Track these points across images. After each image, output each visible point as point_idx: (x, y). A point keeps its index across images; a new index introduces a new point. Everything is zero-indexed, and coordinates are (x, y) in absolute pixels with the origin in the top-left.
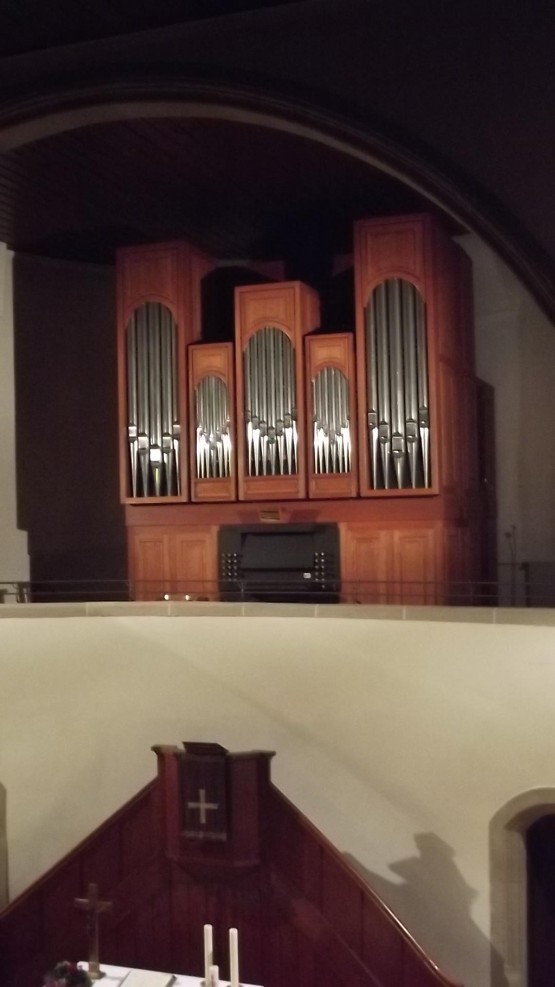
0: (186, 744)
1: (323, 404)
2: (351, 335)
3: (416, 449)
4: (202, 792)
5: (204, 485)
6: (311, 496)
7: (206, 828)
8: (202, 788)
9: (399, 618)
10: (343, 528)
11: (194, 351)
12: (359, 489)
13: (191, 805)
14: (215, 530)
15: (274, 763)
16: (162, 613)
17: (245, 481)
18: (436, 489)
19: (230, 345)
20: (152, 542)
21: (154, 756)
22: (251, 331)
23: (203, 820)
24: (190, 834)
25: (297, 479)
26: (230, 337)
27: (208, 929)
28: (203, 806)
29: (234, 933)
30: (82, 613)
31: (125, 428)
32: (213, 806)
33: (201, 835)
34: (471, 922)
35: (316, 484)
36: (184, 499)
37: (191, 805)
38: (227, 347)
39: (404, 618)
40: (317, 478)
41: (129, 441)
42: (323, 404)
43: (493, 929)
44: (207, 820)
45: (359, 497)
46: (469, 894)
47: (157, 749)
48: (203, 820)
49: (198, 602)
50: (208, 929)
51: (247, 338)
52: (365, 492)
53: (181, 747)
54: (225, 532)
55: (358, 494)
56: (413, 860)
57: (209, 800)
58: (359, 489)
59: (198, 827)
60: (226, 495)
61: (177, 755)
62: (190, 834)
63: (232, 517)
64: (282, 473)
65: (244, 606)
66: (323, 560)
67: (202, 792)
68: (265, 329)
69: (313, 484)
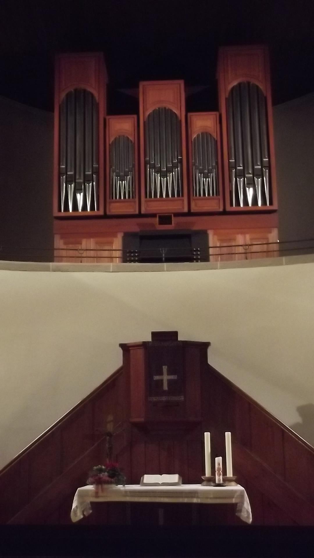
1: (199, 157)
2: (135, 116)
3: (261, 182)
4: (165, 368)
5: (118, 204)
7: (169, 393)
8: (165, 365)
9: (281, 264)
10: (211, 233)
11: (110, 120)
13: (156, 378)
21: (120, 351)
22: (149, 111)
23: (165, 387)
24: (154, 399)
25: (183, 200)
26: (137, 112)
27: (207, 435)
28: (166, 378)
29: (228, 435)
30: (47, 269)
32: (172, 377)
33: (164, 399)
36: (101, 213)
37: (156, 378)
40: (194, 199)
44: (168, 387)
45: (225, 213)
47: (124, 347)
48: (165, 387)
50: (207, 435)
52: (228, 209)
53: (149, 339)
54: (128, 237)
59: (164, 393)
61: (144, 344)
62: (154, 399)
63: (133, 226)
64: (176, 196)
65: (165, 265)
66: (199, 253)
67: (165, 368)
68: (146, 197)
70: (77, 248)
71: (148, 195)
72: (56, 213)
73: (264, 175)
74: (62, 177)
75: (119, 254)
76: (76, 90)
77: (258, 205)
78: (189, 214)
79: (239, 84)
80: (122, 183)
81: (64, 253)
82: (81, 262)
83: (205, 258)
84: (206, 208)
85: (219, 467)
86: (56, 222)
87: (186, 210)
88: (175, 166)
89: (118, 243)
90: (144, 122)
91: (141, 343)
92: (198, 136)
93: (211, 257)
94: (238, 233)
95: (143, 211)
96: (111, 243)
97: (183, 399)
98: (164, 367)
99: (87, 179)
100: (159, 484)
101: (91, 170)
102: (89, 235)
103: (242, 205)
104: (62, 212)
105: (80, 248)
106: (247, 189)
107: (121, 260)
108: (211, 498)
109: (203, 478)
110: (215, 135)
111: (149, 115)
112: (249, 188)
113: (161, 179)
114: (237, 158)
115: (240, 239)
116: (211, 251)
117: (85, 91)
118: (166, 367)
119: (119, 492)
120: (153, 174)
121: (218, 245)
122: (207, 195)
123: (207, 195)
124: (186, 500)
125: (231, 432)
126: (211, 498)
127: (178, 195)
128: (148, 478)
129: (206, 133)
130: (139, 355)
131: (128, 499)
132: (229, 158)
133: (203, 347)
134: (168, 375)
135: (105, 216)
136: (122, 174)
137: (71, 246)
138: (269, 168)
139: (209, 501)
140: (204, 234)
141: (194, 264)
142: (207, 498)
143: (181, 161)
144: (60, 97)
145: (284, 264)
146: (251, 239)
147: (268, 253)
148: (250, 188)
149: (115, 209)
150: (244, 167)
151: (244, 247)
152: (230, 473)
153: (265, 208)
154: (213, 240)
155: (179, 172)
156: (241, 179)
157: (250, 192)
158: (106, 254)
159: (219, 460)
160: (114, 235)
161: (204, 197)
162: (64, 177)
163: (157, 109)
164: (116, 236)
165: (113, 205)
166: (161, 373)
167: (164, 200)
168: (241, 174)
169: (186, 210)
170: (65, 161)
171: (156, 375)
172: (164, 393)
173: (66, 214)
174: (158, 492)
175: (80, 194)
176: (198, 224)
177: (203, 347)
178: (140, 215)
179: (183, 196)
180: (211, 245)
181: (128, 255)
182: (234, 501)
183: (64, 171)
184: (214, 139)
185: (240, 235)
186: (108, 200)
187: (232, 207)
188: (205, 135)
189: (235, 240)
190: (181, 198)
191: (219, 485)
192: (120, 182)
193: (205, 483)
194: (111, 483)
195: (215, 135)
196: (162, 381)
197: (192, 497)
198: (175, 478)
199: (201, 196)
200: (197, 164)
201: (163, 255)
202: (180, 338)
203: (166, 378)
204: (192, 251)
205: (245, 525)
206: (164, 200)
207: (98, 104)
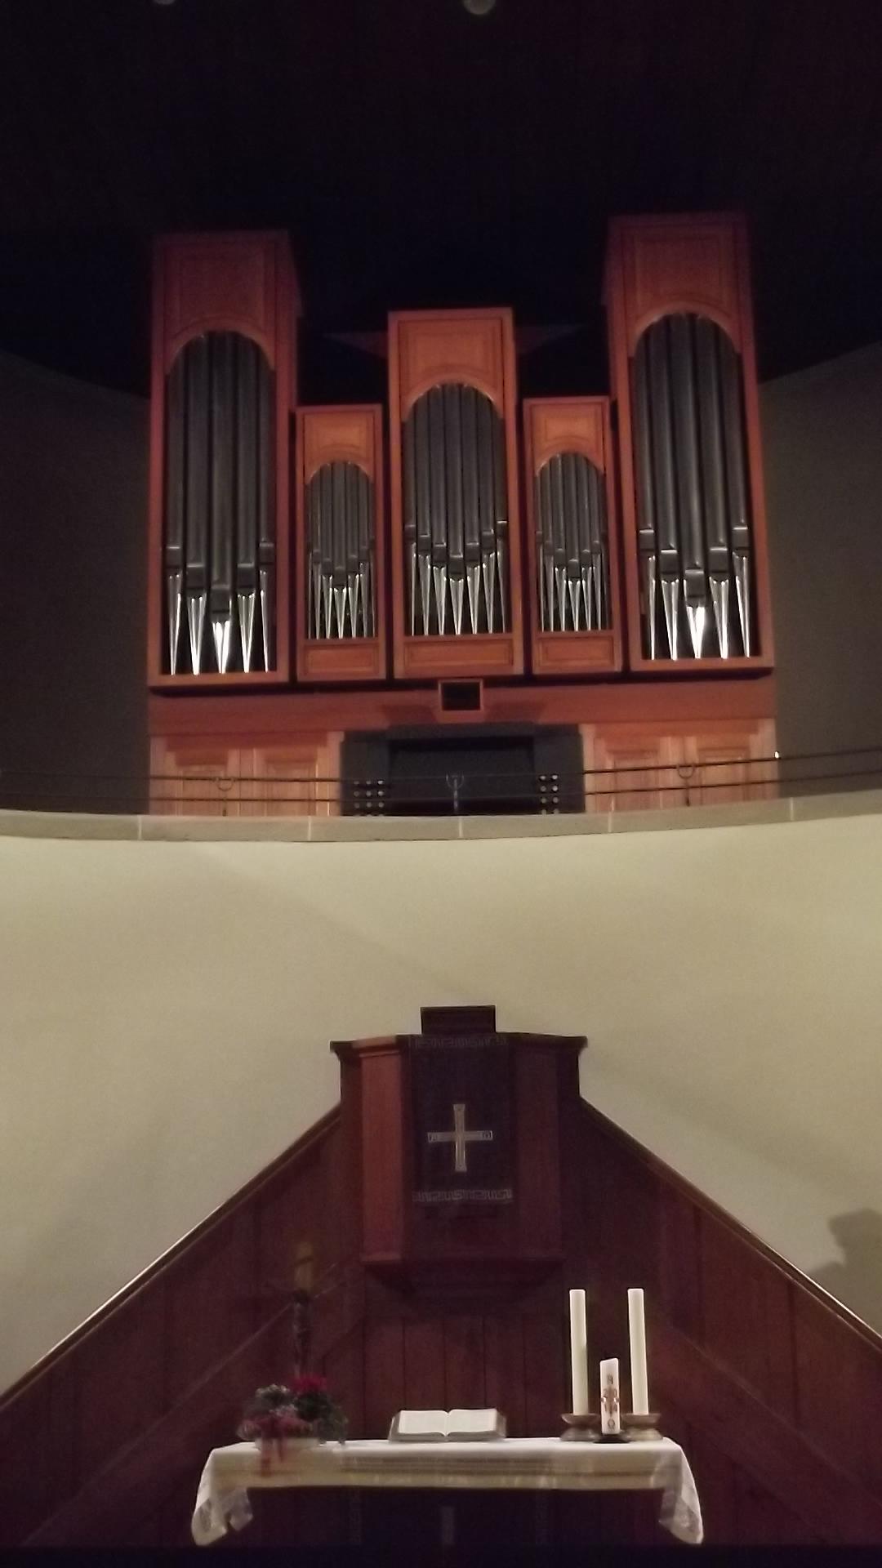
0: (430, 1016)
1: (555, 522)
4: (459, 1111)
6: (537, 671)
7: (471, 1179)
8: (460, 1101)
10: (588, 732)
13: (435, 1137)
14: (335, 740)
16: (296, 836)
17: (407, 645)
19: (378, 408)
20: (605, 469)
21: (335, 1063)
23: (461, 1163)
24: (427, 1197)
27: (577, 1298)
28: (461, 1137)
29: (636, 1297)
30: (130, 835)
32: (479, 1136)
33: (457, 1196)
35: (546, 651)
36: (282, 675)
37: (435, 1137)
38: (372, 411)
39: (792, 816)
42: (555, 522)
45: (627, 676)
47: (342, 1049)
48: (461, 1163)
49: (638, 616)
50: (577, 1298)
52: (638, 664)
53: (414, 1027)
54: (355, 743)
57: (470, 1125)
59: (458, 1181)
60: (365, 669)
61: (402, 1044)
63: (371, 713)
65: (460, 822)
67: (459, 1111)
72: (155, 678)
73: (737, 570)
74: (171, 577)
75: (331, 790)
76: (211, 335)
78: (529, 679)
79: (667, 321)
80: (341, 593)
81: (178, 789)
83: (573, 803)
87: (518, 669)
88: (487, 546)
89: (328, 760)
90: (403, 426)
91: (394, 1041)
92: (552, 462)
94: (664, 734)
95: (399, 672)
96: (310, 761)
97: (508, 1194)
98: (456, 1107)
99: (244, 583)
100: (443, 1435)
102: (248, 739)
106: (689, 609)
108: (586, 1475)
110: (601, 460)
112: (695, 607)
115: (671, 750)
116: (590, 783)
119: (329, 1458)
124: (517, 1482)
126: (586, 1475)
127: (603, 626)
128: (410, 1421)
129: (576, 455)
130: (386, 1076)
133: (567, 1051)
135: (294, 687)
139: (584, 1484)
140: (568, 736)
141: (544, 817)
142: (578, 1475)
143: (504, 533)
146: (701, 750)
147: (747, 788)
148: (697, 607)
149: (320, 665)
152: (641, 1405)
153: (738, 664)
154: (593, 751)
157: (222, 634)
158: (295, 790)
159: (609, 1367)
160: (319, 737)
161: (570, 634)
162: (178, 576)
163: (438, 386)
165: (316, 656)
166: (447, 1124)
167: (459, 642)
168: (673, 569)
169: (518, 669)
170: (180, 531)
171: (436, 1130)
172: (458, 1181)
173: (183, 680)
174: (440, 1460)
175: (223, 622)
176: (553, 706)
177: (567, 1051)
178: (390, 684)
179: (509, 628)
180: (588, 764)
182: (652, 1482)
183: (178, 561)
184: (597, 471)
185: (669, 738)
186: (301, 641)
188: (572, 461)
189: (655, 751)
192: (336, 590)
195: (601, 460)
196: (451, 1145)
197: (535, 1473)
198: (486, 1419)
200: (550, 542)
202: (503, 1026)
203: (461, 1137)
206: (459, 642)
207: (273, 375)
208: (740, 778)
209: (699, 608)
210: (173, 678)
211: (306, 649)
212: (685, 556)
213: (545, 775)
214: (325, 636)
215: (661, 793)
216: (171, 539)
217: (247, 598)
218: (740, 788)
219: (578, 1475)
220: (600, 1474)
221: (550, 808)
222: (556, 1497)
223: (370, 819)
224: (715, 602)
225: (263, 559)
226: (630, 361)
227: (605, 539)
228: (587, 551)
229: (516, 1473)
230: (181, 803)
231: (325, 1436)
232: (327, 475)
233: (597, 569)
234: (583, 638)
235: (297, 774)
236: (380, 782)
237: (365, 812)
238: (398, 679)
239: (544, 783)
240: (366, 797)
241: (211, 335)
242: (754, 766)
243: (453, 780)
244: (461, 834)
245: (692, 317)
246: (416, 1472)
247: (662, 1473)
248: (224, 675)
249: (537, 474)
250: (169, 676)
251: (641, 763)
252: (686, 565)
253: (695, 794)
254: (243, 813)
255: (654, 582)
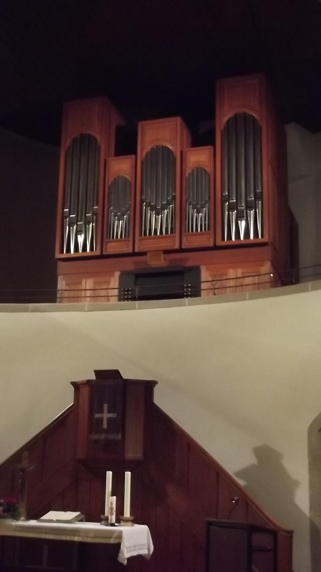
0: (98, 373)
2: (211, 147)
4: (106, 406)
7: (107, 431)
9: (244, 299)
12: (215, 240)
13: (97, 416)
14: (117, 274)
15: (157, 390)
16: (81, 310)
17: (140, 240)
18: (266, 239)
19: (133, 156)
21: (72, 389)
22: (148, 149)
23: (105, 426)
24: (94, 437)
25: (174, 237)
27: (109, 474)
28: (106, 415)
29: (128, 475)
30: (27, 310)
31: (61, 211)
32: (111, 415)
33: (103, 437)
34: (296, 506)
37: (97, 416)
38: (131, 158)
41: (63, 217)
43: (311, 508)
45: (216, 248)
46: (296, 484)
47: (74, 384)
48: (105, 426)
50: (109, 474)
51: (145, 153)
52: (219, 243)
53: (93, 377)
54: (124, 275)
55: (215, 244)
56: (253, 466)
58: (215, 240)
61: (89, 382)
62: (94, 437)
63: (129, 264)
65: (137, 303)
67: (106, 406)
69: (184, 240)
70: (78, 289)
71: (143, 233)
72: (58, 255)
73: (257, 206)
74: (65, 220)
75: (116, 292)
76: (81, 135)
77: (250, 238)
78: (181, 250)
79: (236, 116)
80: (199, 215)
81: (66, 294)
82: (61, 302)
83: (196, 293)
84: (196, 244)
85: (111, 507)
86: (60, 264)
88: (168, 204)
89: (115, 282)
90: (142, 162)
91: (86, 382)
92: (193, 170)
93: (202, 292)
94: (230, 268)
95: (136, 250)
96: (108, 282)
97: (120, 437)
98: (105, 405)
99: (250, 206)
100: (53, 520)
101: (91, 212)
102: (89, 274)
103: (233, 239)
104: (64, 253)
105: (80, 288)
106: (239, 222)
107: (116, 298)
108: (91, 537)
109: (102, 517)
110: (209, 169)
111: (147, 154)
112: (241, 221)
113: (155, 217)
114: (230, 192)
115: (231, 273)
116: (203, 286)
117: (89, 136)
118: (107, 405)
119: (10, 526)
120: (148, 212)
121: (210, 279)
122: (203, 230)
123: (203, 230)
124: (68, 538)
125: (112, 471)
127: (172, 232)
128: (52, 515)
129: (201, 168)
130: (85, 391)
131: (18, 534)
132: (222, 191)
134: (109, 412)
135: (102, 257)
136: (199, 206)
137: (72, 287)
138: (262, 199)
139: (89, 540)
140: (196, 270)
141: (186, 300)
142: (87, 537)
143: (174, 198)
144: (66, 142)
145: (30, 311)
146: (243, 273)
147: (259, 285)
148: (242, 220)
149: (112, 248)
150: (237, 200)
151: (213, 282)
152: (127, 513)
153: (257, 241)
154: (205, 275)
155: (173, 209)
156: (234, 212)
157: (243, 224)
158: (103, 293)
161: (197, 233)
162: (67, 219)
163: (155, 147)
164: (113, 276)
165: (110, 245)
166: (102, 412)
167: (158, 238)
168: (231, 208)
169: (177, 246)
170: (68, 204)
171: (97, 413)
173: (229, 243)
175: (81, 235)
176: (191, 260)
178: (134, 254)
179: (129, 237)
180: (203, 279)
181: (126, 293)
182: (112, 541)
183: (67, 215)
184: (208, 173)
185: (232, 270)
186: (105, 241)
187: (224, 242)
188: (199, 170)
189: (226, 274)
190: (173, 235)
191: (113, 525)
192: (197, 214)
193: (103, 522)
194: (4, 517)
195: (209, 170)
196: (102, 419)
197: (74, 535)
198: (71, 515)
199: (146, 235)
200: (191, 200)
201: (137, 293)
203: (106, 415)
204: (183, 288)
205: (122, 564)
206: (158, 238)
207: (100, 147)
208: (257, 282)
209: (82, 235)
210: (65, 255)
211: (107, 243)
212: (239, 202)
213: (186, 284)
214: (118, 238)
215: (228, 289)
216: (65, 207)
217: (73, 228)
218: (205, 291)
219: (87, 537)
220: (95, 537)
221: (187, 296)
222: (82, 545)
223: (126, 302)
224: (249, 219)
225: (94, 212)
226: (222, 132)
227: (209, 198)
228: (203, 202)
229: (68, 535)
230: (66, 299)
231: (16, 517)
232: (116, 181)
233: (207, 209)
234: (201, 234)
235: (104, 287)
236: (189, 285)
237: (127, 299)
238: (183, 249)
239: (130, 291)
240: (125, 294)
241: (81, 135)
242: (262, 277)
243: (136, 288)
244: (187, 305)
245: (245, 114)
246: (37, 533)
247: (116, 538)
248: (234, 241)
249: (187, 175)
250: (224, 241)
251: (221, 278)
252: (239, 205)
253: (217, 291)
254: (69, 302)
255: (227, 212)
